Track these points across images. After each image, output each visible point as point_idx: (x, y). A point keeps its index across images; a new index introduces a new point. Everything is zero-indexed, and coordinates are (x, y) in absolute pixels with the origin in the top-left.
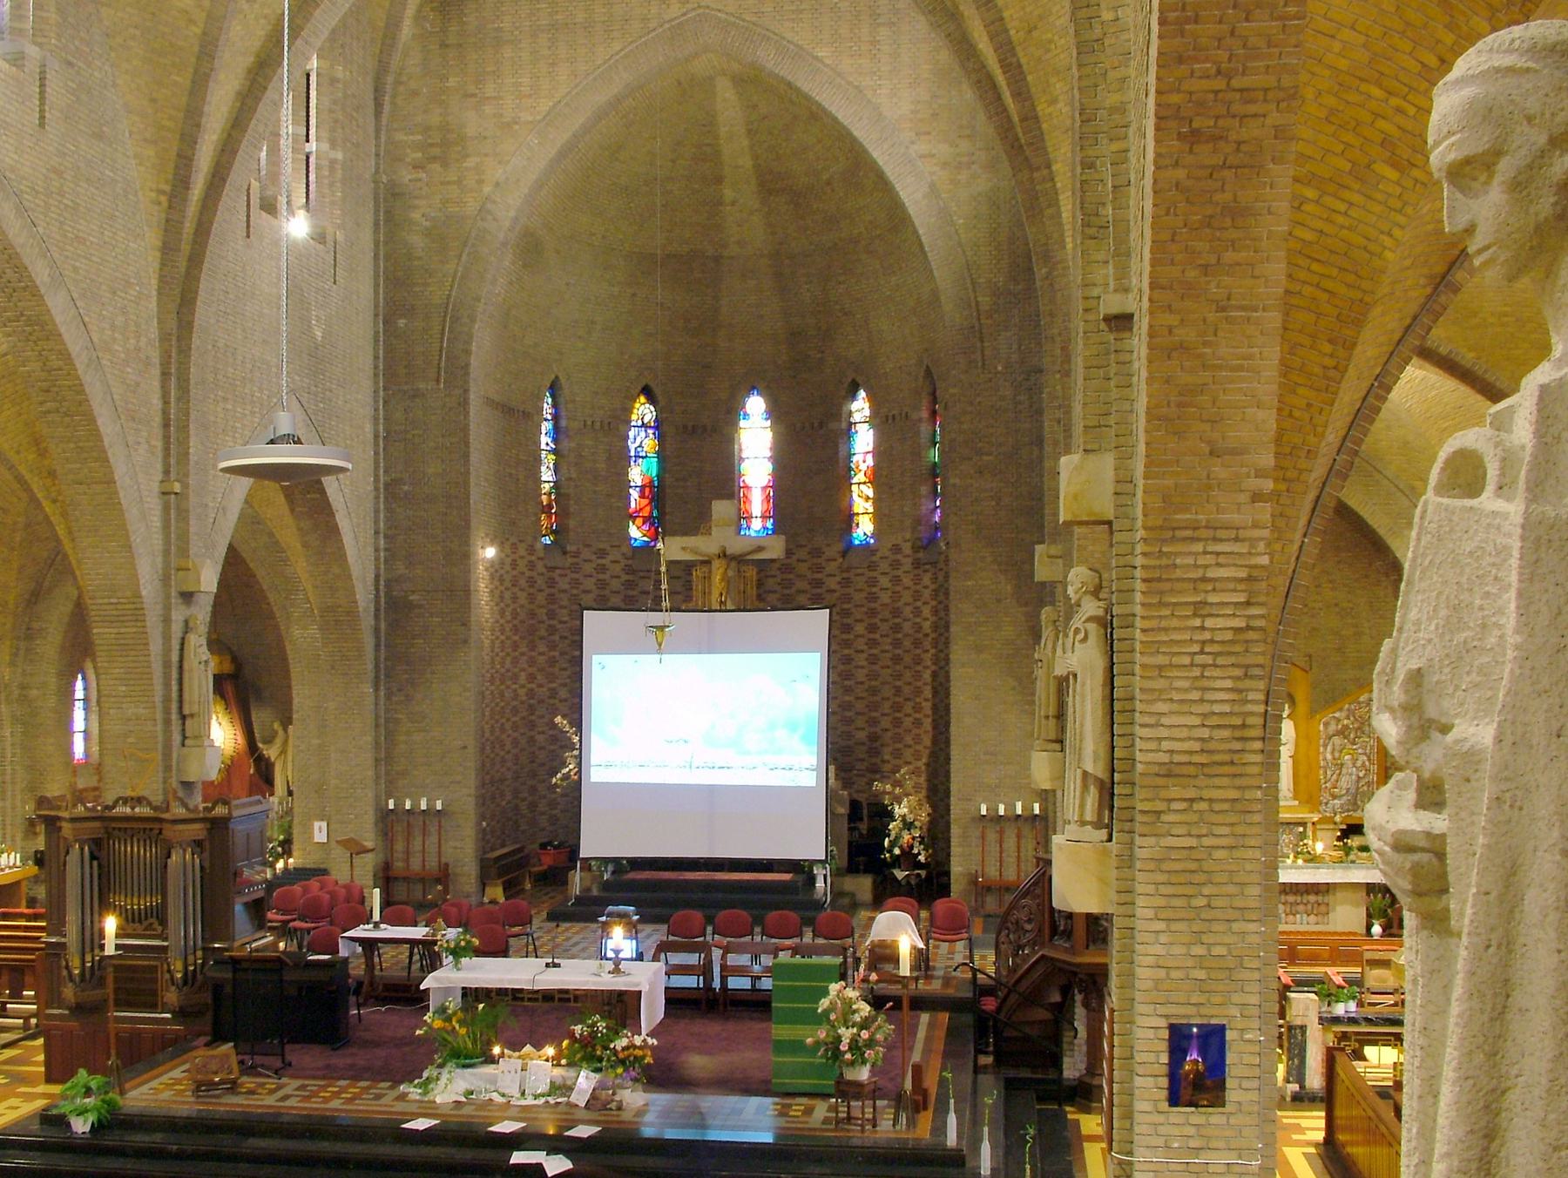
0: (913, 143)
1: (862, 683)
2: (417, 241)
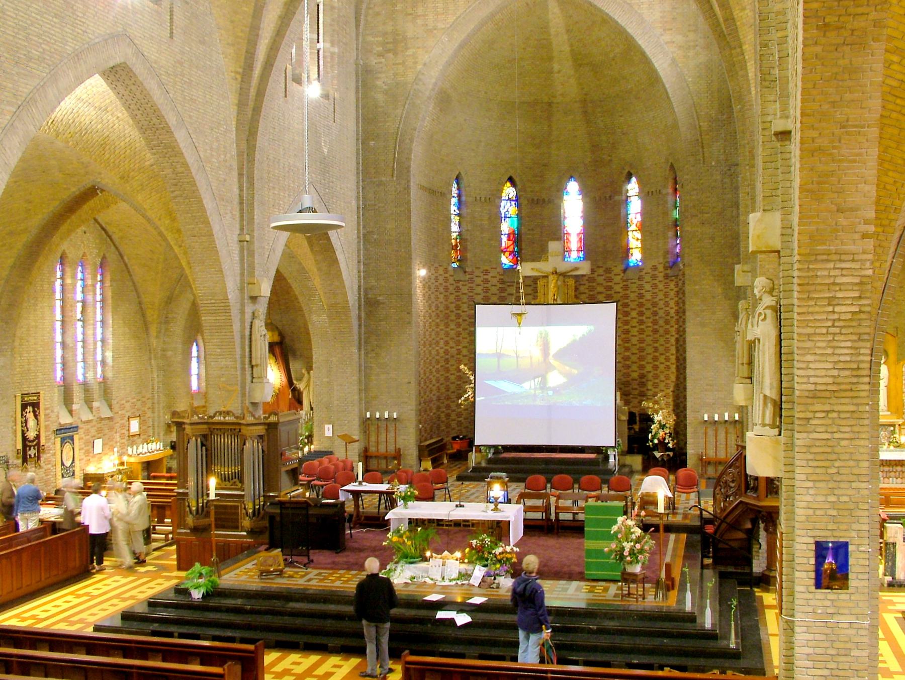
0: (662, 35)
1: (635, 345)
2: (380, 97)
